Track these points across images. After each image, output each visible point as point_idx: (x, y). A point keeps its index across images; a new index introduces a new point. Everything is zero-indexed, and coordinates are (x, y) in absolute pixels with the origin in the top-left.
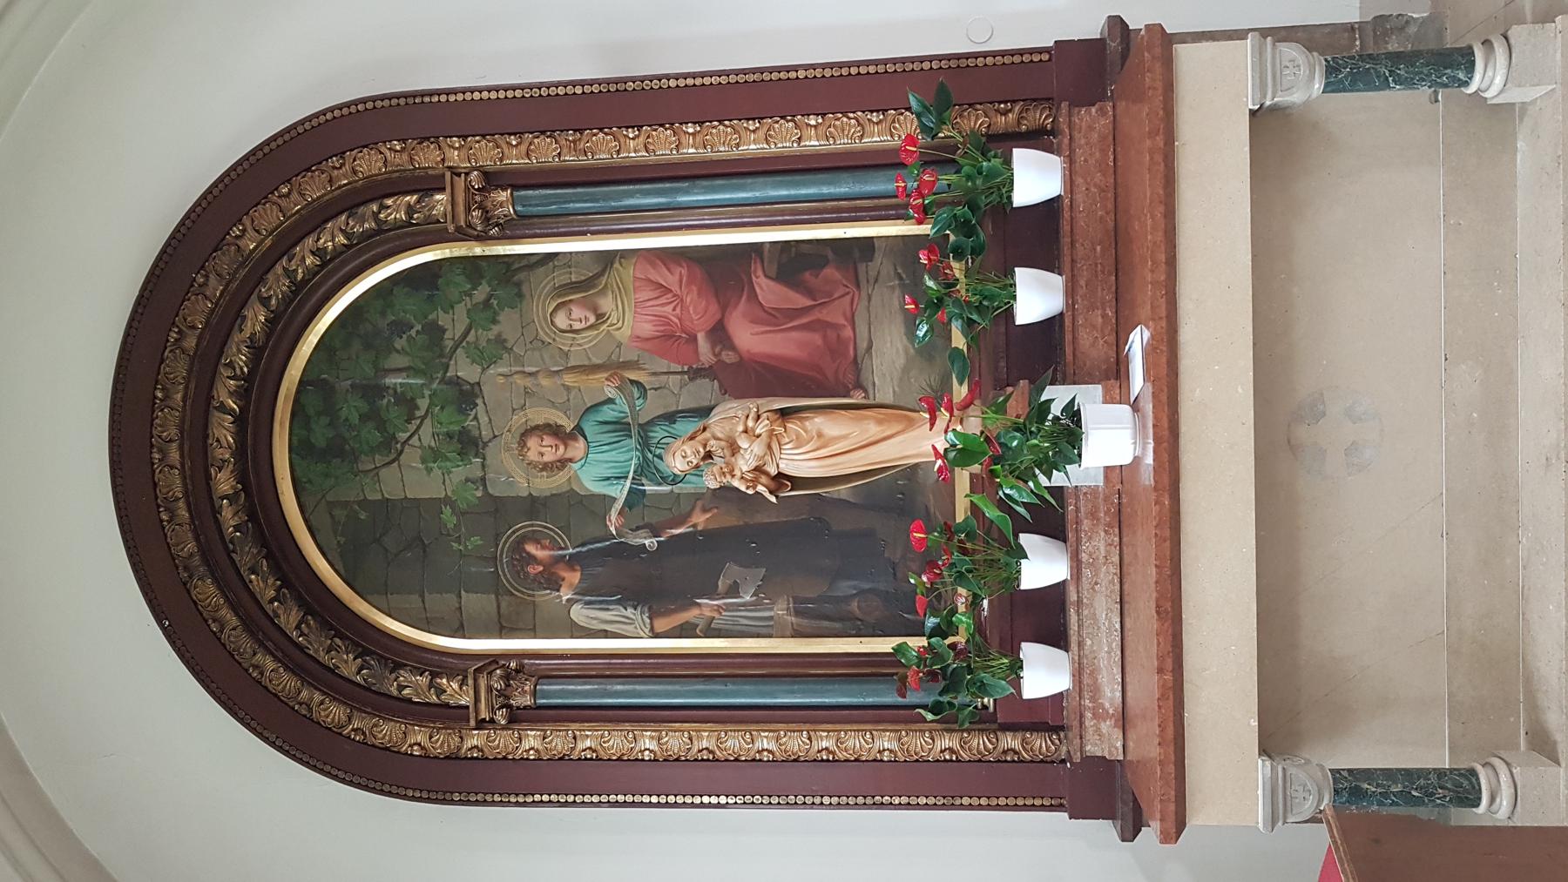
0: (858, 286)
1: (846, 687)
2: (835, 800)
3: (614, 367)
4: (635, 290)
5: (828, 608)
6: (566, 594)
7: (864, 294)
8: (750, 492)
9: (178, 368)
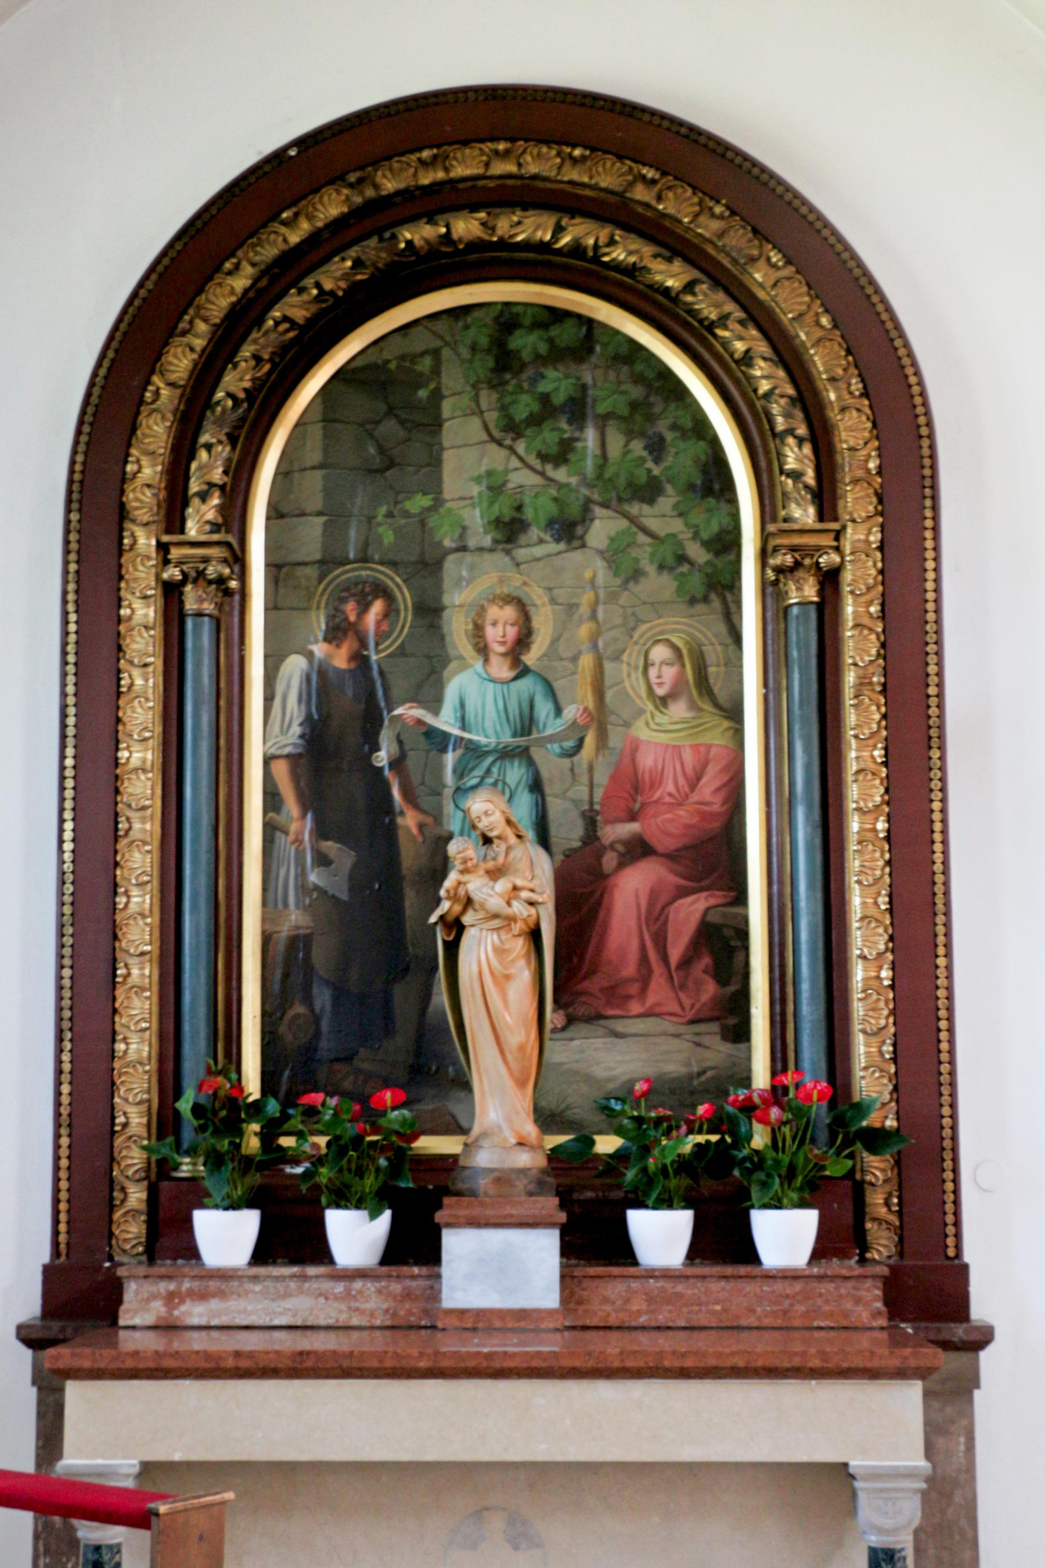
0: (693, 1022)
2: (67, 983)
3: (600, 718)
4: (695, 747)
5: (297, 978)
6: (320, 649)
7: (682, 1029)
8: (442, 893)
9: (608, 176)
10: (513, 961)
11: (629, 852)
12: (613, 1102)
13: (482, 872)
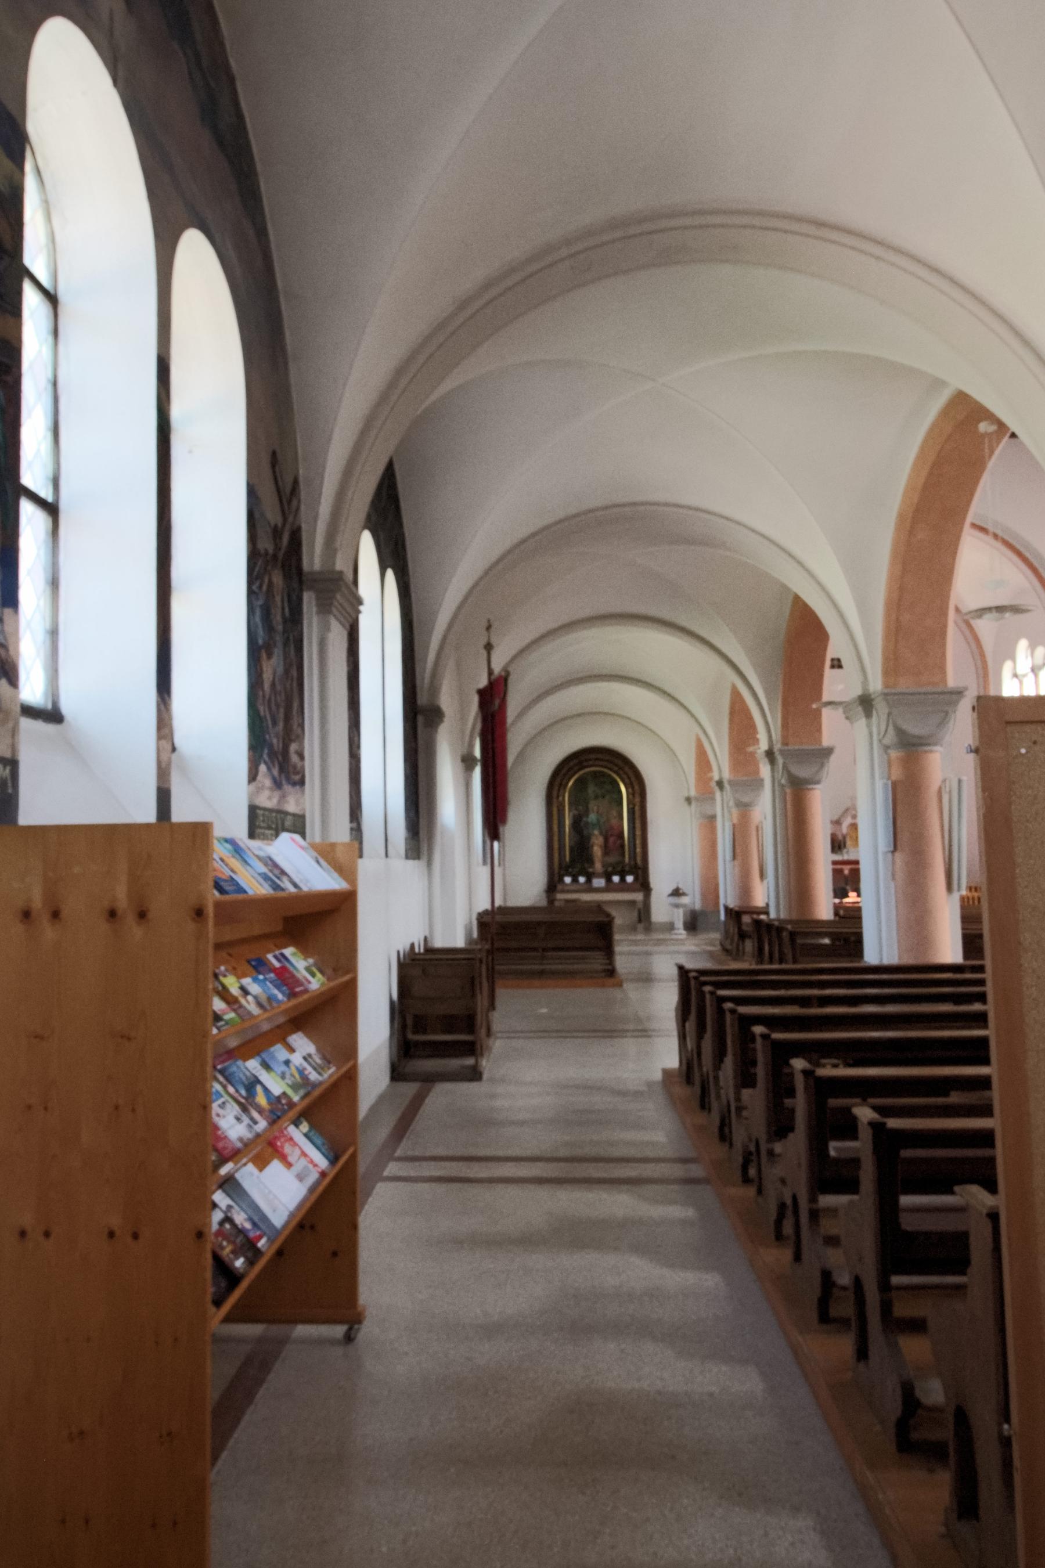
1: (886, 799)
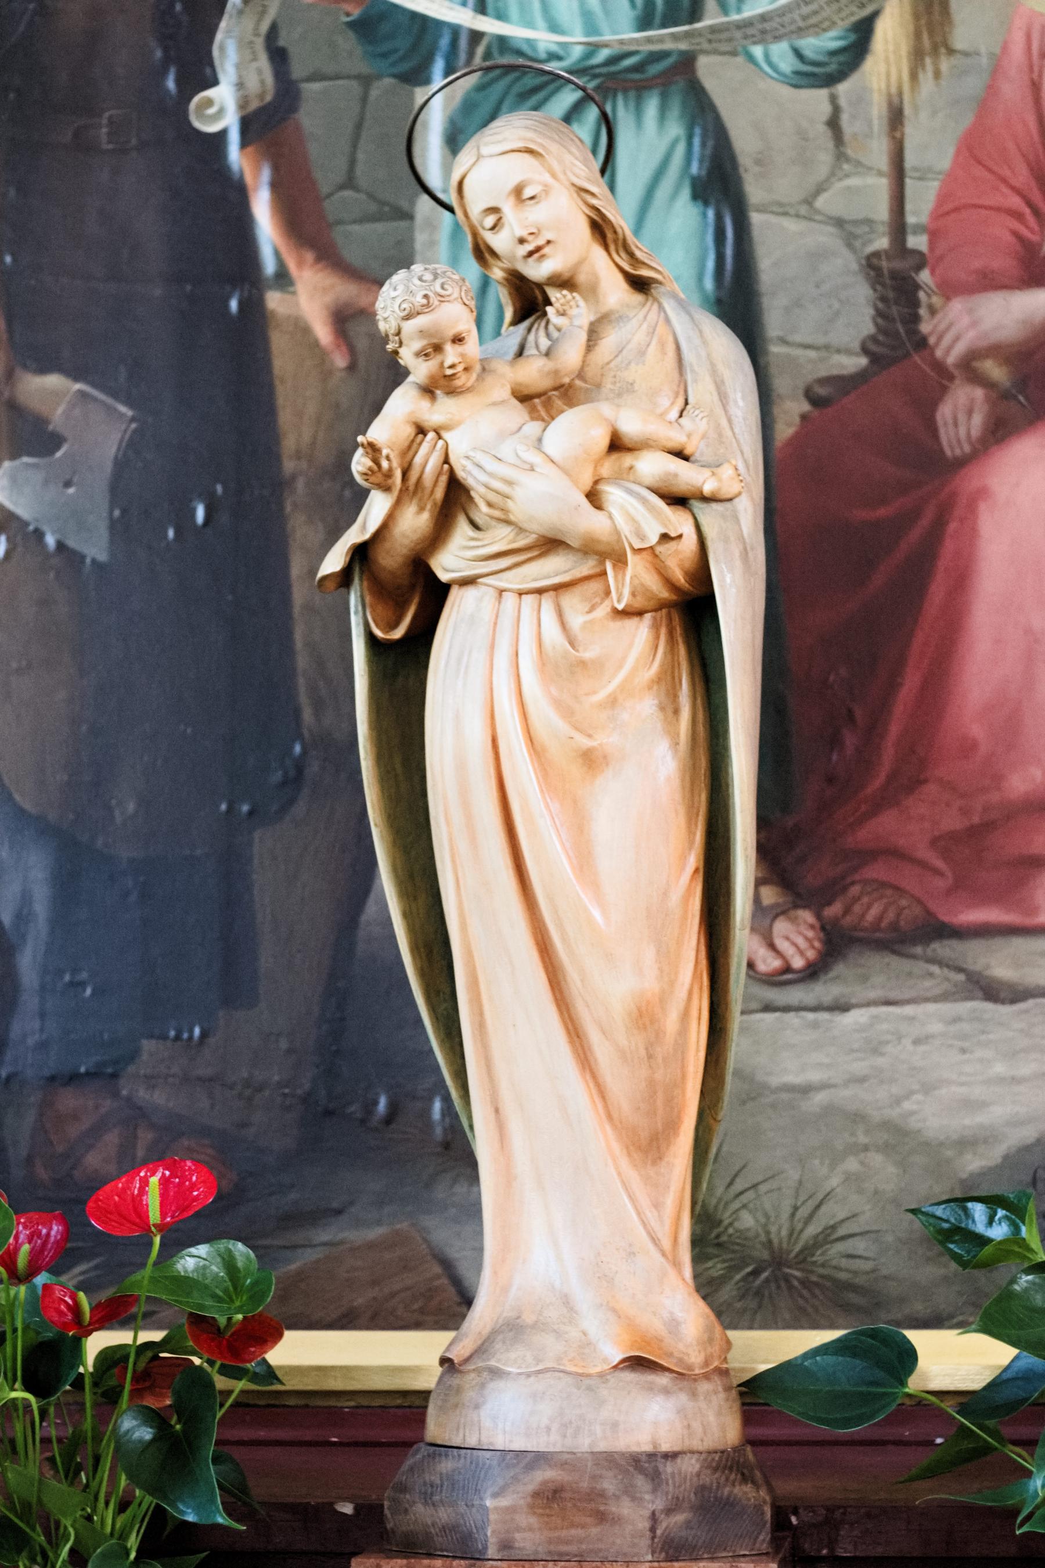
10: (613, 702)
11: (1022, 383)
12: (978, 1210)
13: (503, 392)
